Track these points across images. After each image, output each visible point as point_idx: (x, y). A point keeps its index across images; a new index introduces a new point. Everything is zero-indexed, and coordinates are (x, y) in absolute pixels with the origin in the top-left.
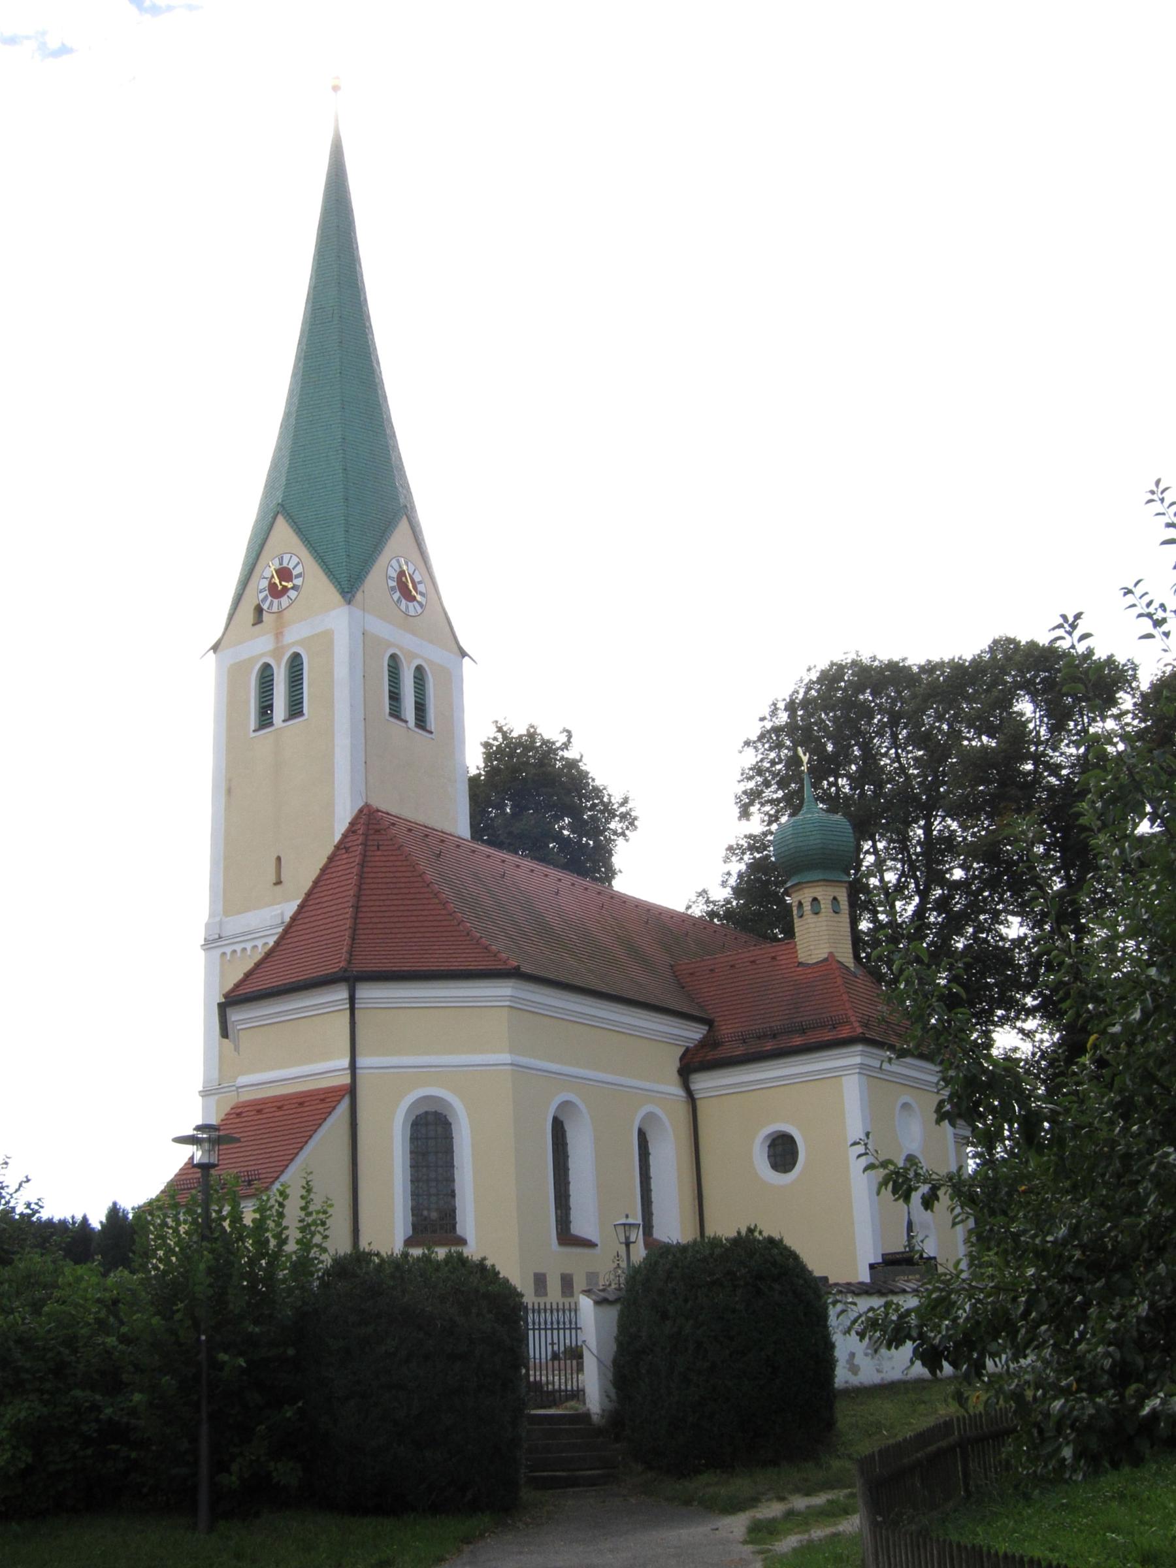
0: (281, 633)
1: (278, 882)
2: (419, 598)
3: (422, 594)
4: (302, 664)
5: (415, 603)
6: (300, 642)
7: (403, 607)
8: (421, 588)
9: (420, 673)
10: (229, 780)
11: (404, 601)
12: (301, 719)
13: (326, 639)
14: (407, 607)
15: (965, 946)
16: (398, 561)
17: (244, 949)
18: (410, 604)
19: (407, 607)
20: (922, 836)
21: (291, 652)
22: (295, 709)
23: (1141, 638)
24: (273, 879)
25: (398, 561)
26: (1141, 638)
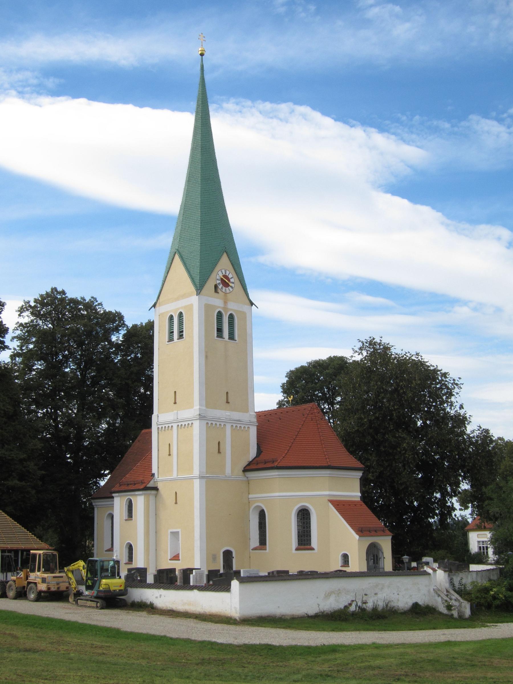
0: (227, 302)
1: (175, 403)
2: (231, 284)
3: (233, 283)
4: (183, 316)
5: (230, 288)
6: (182, 308)
7: (224, 290)
8: (232, 280)
9: (231, 317)
10: (206, 352)
11: (224, 288)
12: (172, 342)
13: (190, 307)
14: (226, 290)
15: (449, 506)
16: (222, 271)
17: (169, 427)
18: (227, 289)
19: (226, 290)
20: (421, 547)
21: (169, 315)
22: (181, 336)
23: (149, 310)
24: (173, 402)
25: (222, 271)
26: (149, 310)
